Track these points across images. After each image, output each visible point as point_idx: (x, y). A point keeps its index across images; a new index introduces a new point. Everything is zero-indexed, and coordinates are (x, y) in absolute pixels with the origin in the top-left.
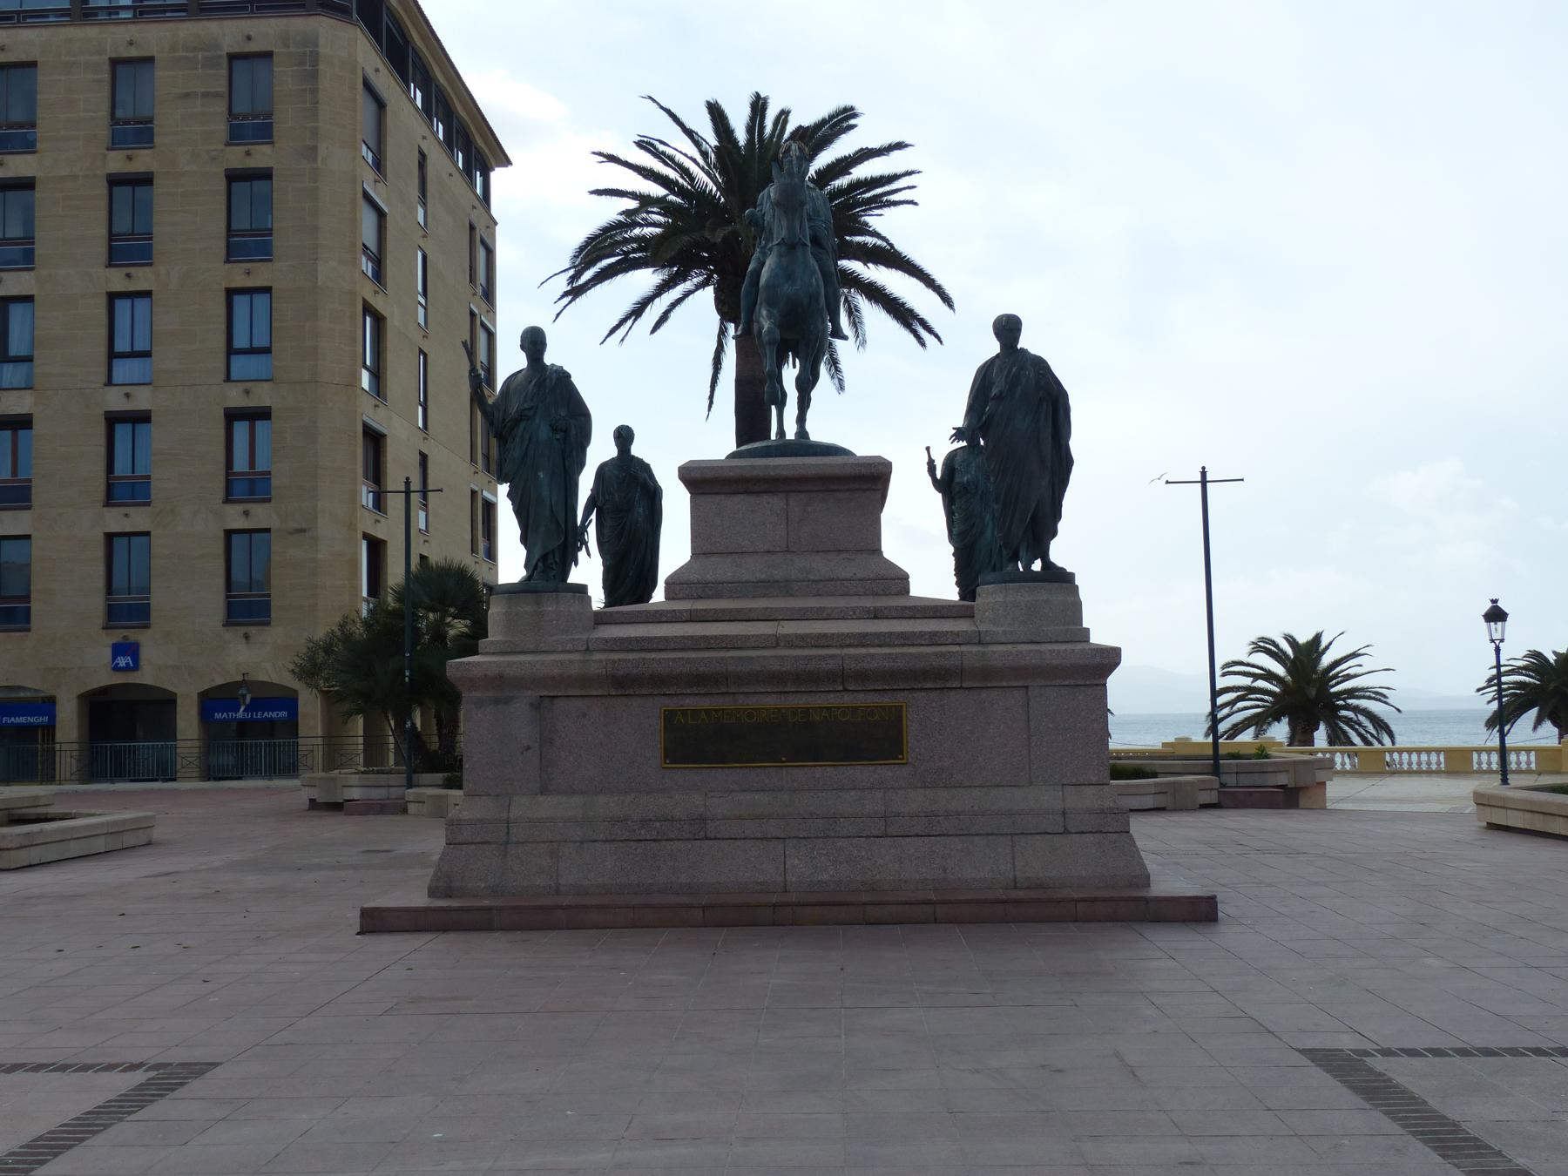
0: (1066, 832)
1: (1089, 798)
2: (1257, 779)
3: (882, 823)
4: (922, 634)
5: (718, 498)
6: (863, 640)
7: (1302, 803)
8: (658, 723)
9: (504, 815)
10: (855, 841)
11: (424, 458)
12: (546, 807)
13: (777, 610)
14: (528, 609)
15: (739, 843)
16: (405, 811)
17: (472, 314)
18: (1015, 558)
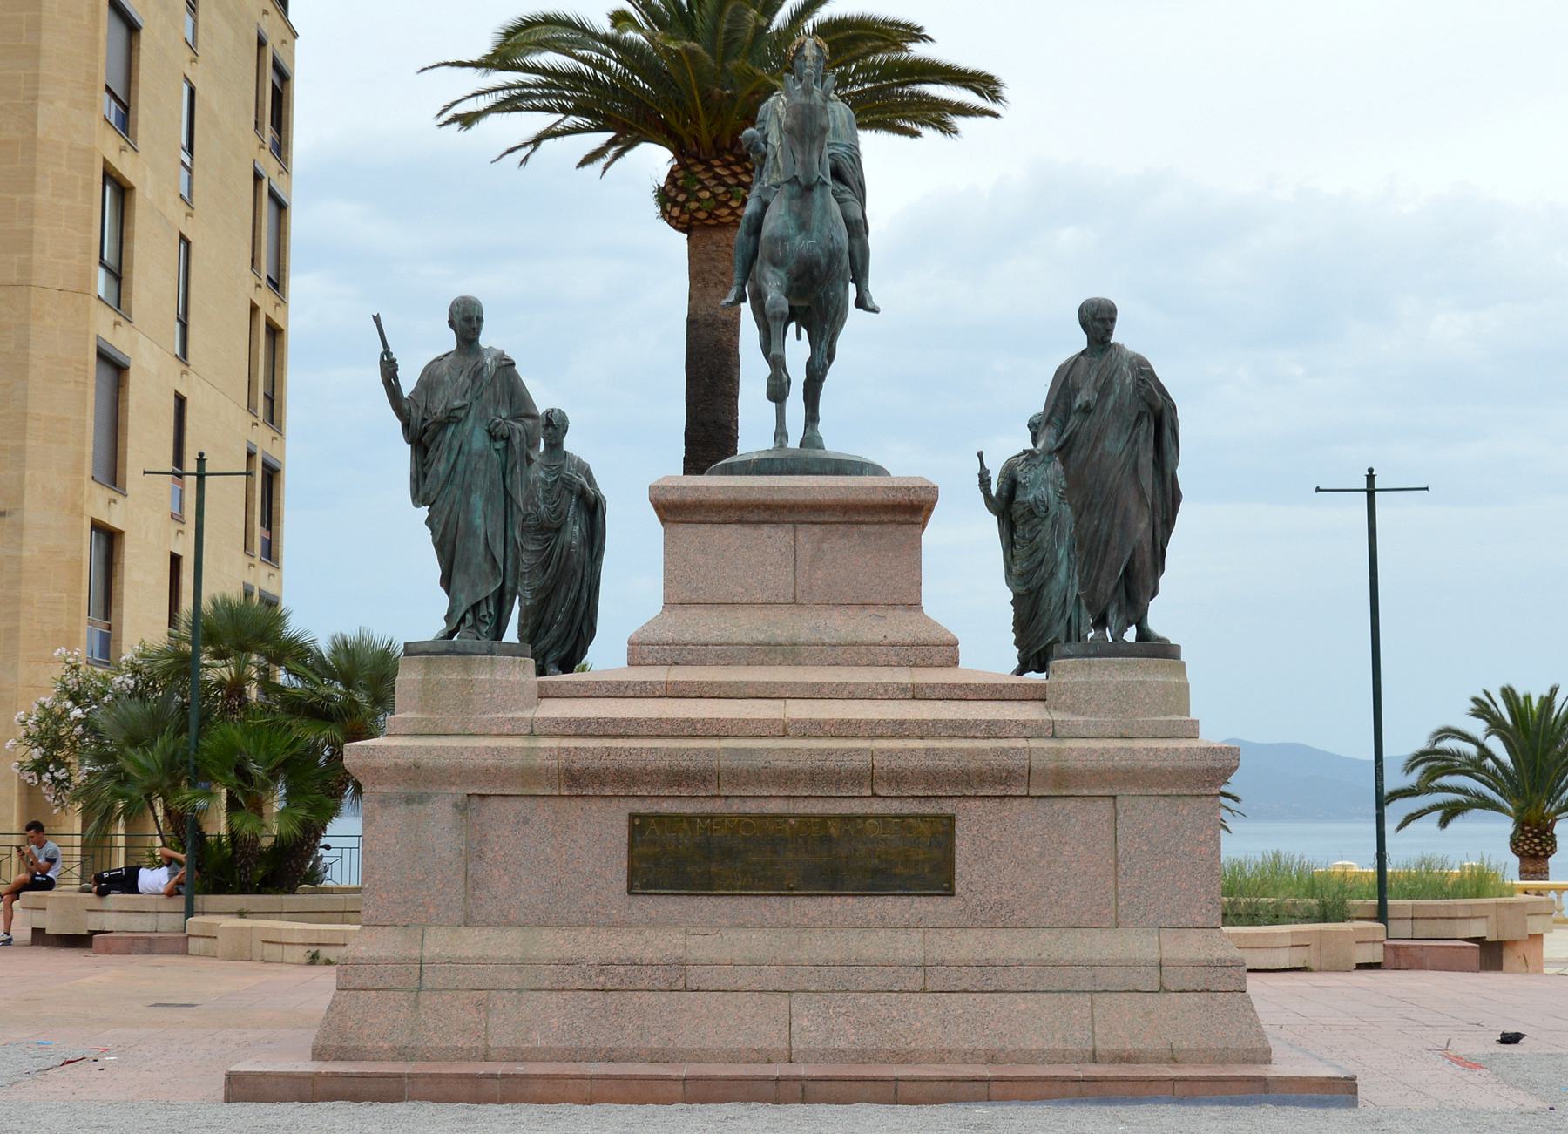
0: (1163, 989)
1: (1190, 947)
2: (1441, 928)
3: (920, 973)
4: (976, 724)
5: (702, 528)
6: (900, 729)
7: (1506, 962)
9: (416, 953)
10: (884, 996)
11: (180, 401)
12: (472, 943)
13: (783, 684)
14: (454, 676)
15: (728, 996)
16: (185, 952)
17: (258, 178)
18: (1101, 622)
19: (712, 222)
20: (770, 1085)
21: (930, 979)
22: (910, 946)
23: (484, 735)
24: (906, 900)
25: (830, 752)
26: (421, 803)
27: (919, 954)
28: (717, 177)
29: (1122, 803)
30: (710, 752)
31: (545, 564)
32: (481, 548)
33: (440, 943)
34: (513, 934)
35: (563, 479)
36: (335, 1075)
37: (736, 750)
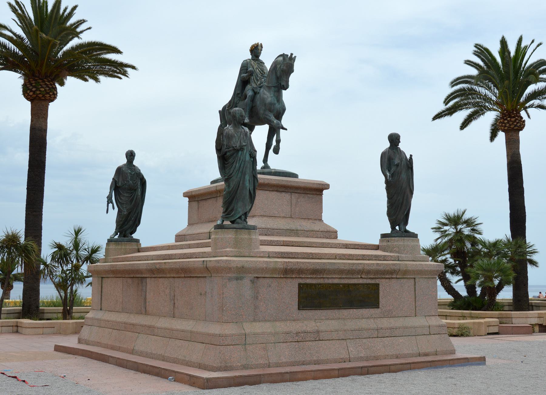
8: (295, 290)
12: (258, 328)
14: (246, 236)
15: (331, 342)
19: (43, 98)
20: (360, 370)
21: (379, 334)
22: (372, 324)
23: (255, 257)
24: (368, 310)
25: (354, 264)
26: (241, 280)
27: (375, 326)
28: (46, 84)
29: (417, 280)
30: (324, 263)
31: (132, 200)
32: (248, 193)
33: (251, 328)
34: (268, 324)
35: (137, 173)
36: (241, 376)
37: (331, 263)
